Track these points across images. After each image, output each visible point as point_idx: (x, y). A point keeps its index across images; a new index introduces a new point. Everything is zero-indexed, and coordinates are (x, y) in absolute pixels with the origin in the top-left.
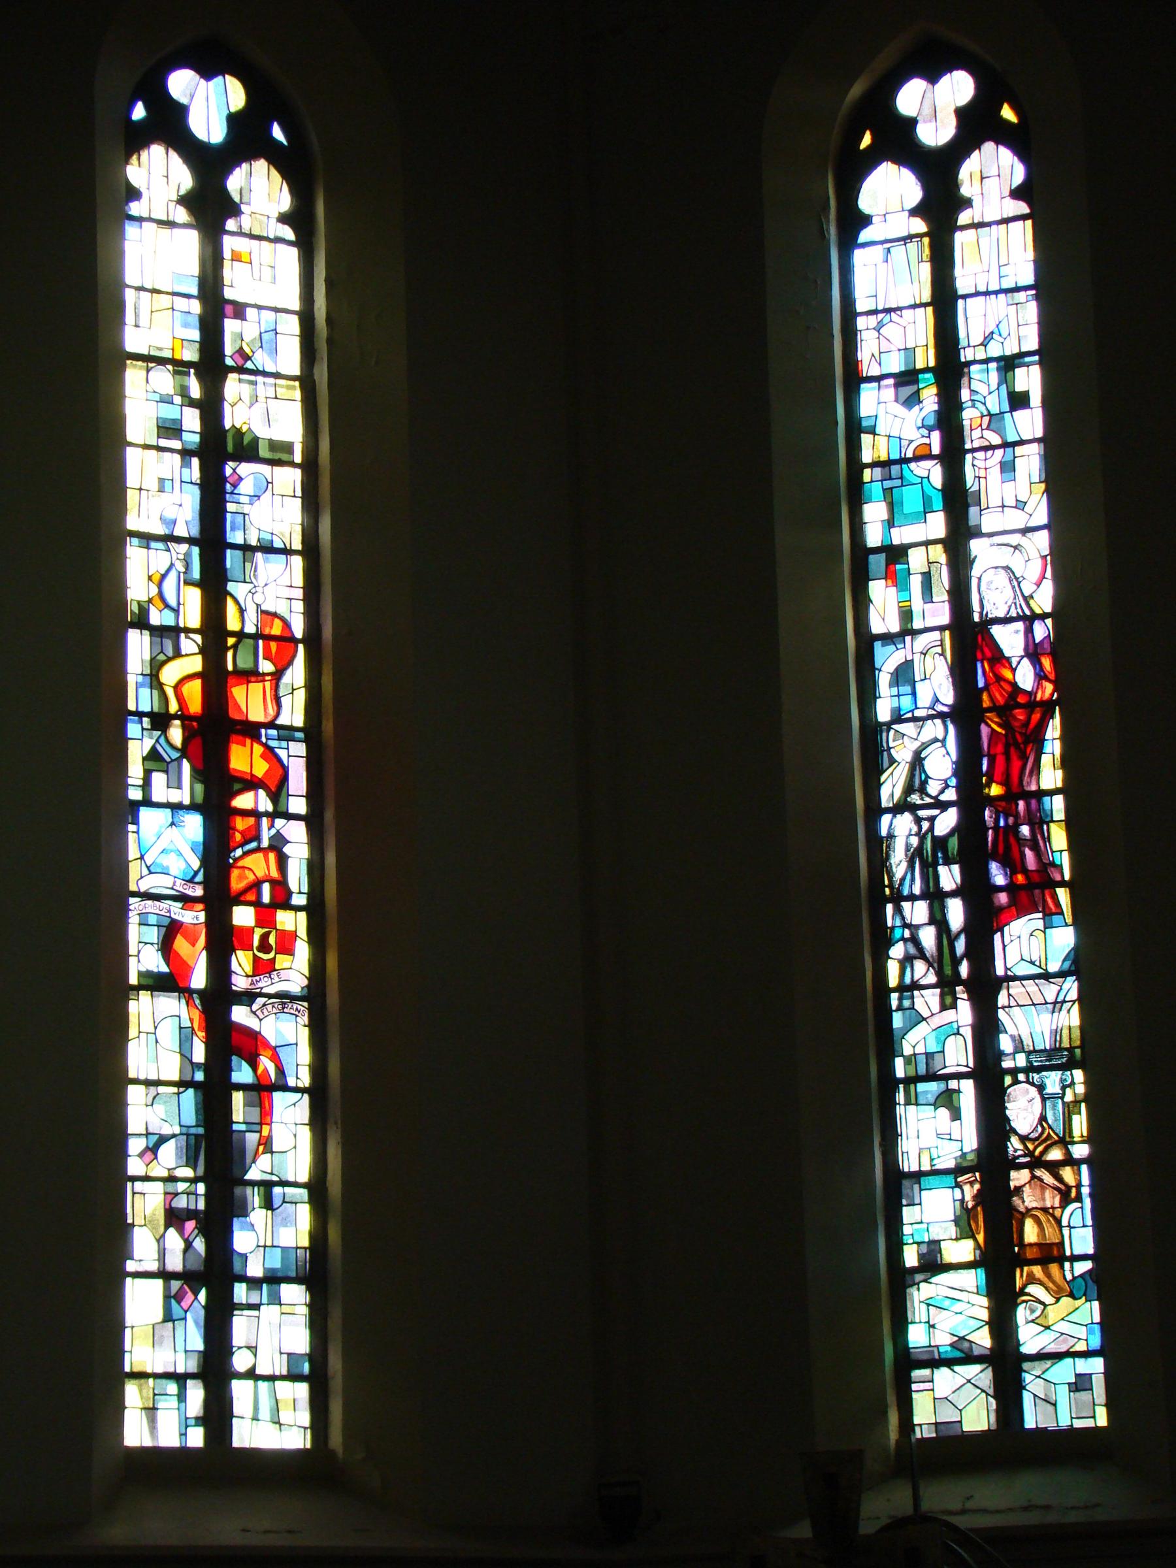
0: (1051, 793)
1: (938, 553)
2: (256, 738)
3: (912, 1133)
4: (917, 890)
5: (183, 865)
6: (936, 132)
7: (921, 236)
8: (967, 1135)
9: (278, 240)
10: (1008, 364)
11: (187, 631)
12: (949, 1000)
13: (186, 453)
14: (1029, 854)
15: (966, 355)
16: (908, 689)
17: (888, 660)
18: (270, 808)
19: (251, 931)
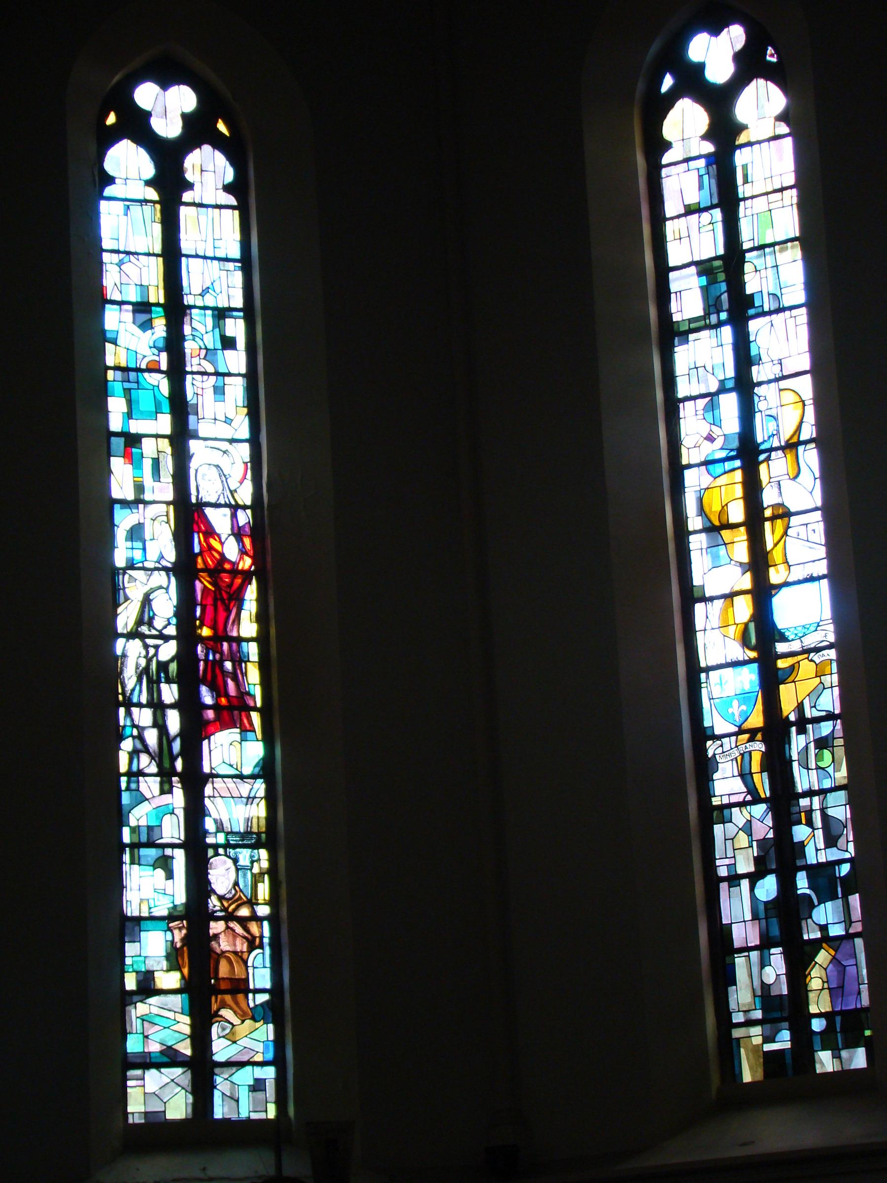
0: (248, 640)
1: (165, 445)
4: (144, 700)
6: (167, 127)
7: (154, 202)
8: (177, 891)
10: (221, 314)
14: (231, 684)
15: (188, 300)
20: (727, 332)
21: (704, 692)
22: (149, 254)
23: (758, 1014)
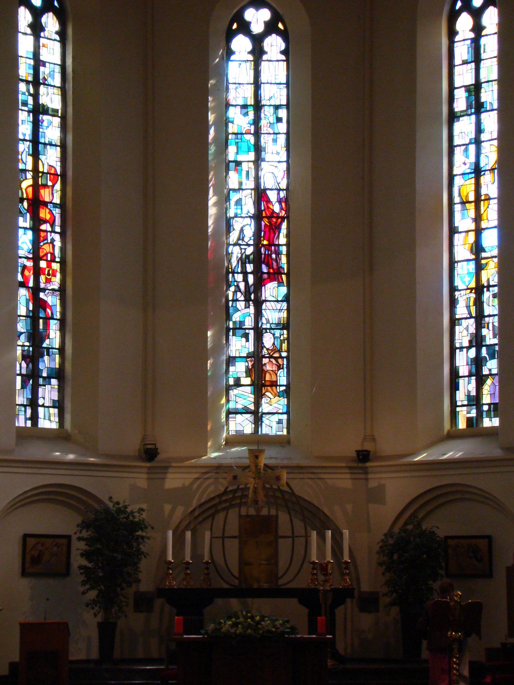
0: (282, 245)
1: (251, 165)
2: (47, 207)
3: (234, 345)
4: (239, 271)
5: (27, 248)
6: (257, 28)
7: (251, 61)
8: (250, 347)
9: (55, 40)
10: (277, 107)
11: (29, 171)
12: (247, 306)
13: (29, 112)
14: (275, 263)
15: (263, 102)
16: (240, 207)
17: (234, 197)
18: (50, 230)
19: (45, 269)
20: (473, 117)
21: (456, 271)
22: (248, 84)
23: (466, 403)
